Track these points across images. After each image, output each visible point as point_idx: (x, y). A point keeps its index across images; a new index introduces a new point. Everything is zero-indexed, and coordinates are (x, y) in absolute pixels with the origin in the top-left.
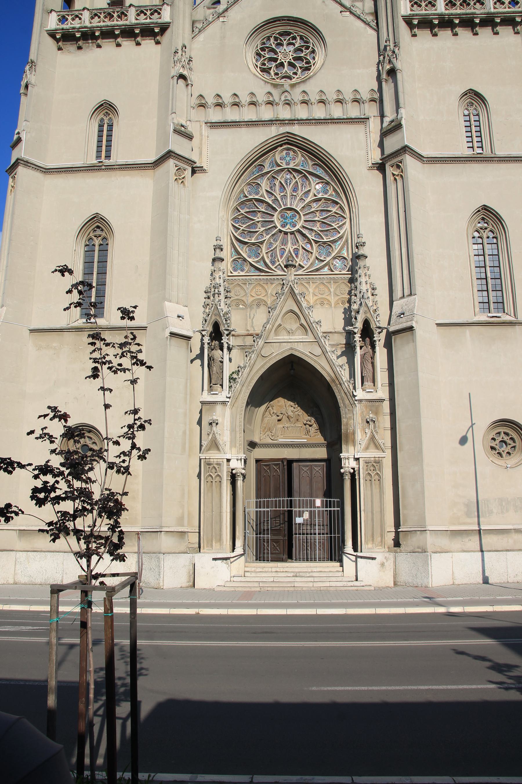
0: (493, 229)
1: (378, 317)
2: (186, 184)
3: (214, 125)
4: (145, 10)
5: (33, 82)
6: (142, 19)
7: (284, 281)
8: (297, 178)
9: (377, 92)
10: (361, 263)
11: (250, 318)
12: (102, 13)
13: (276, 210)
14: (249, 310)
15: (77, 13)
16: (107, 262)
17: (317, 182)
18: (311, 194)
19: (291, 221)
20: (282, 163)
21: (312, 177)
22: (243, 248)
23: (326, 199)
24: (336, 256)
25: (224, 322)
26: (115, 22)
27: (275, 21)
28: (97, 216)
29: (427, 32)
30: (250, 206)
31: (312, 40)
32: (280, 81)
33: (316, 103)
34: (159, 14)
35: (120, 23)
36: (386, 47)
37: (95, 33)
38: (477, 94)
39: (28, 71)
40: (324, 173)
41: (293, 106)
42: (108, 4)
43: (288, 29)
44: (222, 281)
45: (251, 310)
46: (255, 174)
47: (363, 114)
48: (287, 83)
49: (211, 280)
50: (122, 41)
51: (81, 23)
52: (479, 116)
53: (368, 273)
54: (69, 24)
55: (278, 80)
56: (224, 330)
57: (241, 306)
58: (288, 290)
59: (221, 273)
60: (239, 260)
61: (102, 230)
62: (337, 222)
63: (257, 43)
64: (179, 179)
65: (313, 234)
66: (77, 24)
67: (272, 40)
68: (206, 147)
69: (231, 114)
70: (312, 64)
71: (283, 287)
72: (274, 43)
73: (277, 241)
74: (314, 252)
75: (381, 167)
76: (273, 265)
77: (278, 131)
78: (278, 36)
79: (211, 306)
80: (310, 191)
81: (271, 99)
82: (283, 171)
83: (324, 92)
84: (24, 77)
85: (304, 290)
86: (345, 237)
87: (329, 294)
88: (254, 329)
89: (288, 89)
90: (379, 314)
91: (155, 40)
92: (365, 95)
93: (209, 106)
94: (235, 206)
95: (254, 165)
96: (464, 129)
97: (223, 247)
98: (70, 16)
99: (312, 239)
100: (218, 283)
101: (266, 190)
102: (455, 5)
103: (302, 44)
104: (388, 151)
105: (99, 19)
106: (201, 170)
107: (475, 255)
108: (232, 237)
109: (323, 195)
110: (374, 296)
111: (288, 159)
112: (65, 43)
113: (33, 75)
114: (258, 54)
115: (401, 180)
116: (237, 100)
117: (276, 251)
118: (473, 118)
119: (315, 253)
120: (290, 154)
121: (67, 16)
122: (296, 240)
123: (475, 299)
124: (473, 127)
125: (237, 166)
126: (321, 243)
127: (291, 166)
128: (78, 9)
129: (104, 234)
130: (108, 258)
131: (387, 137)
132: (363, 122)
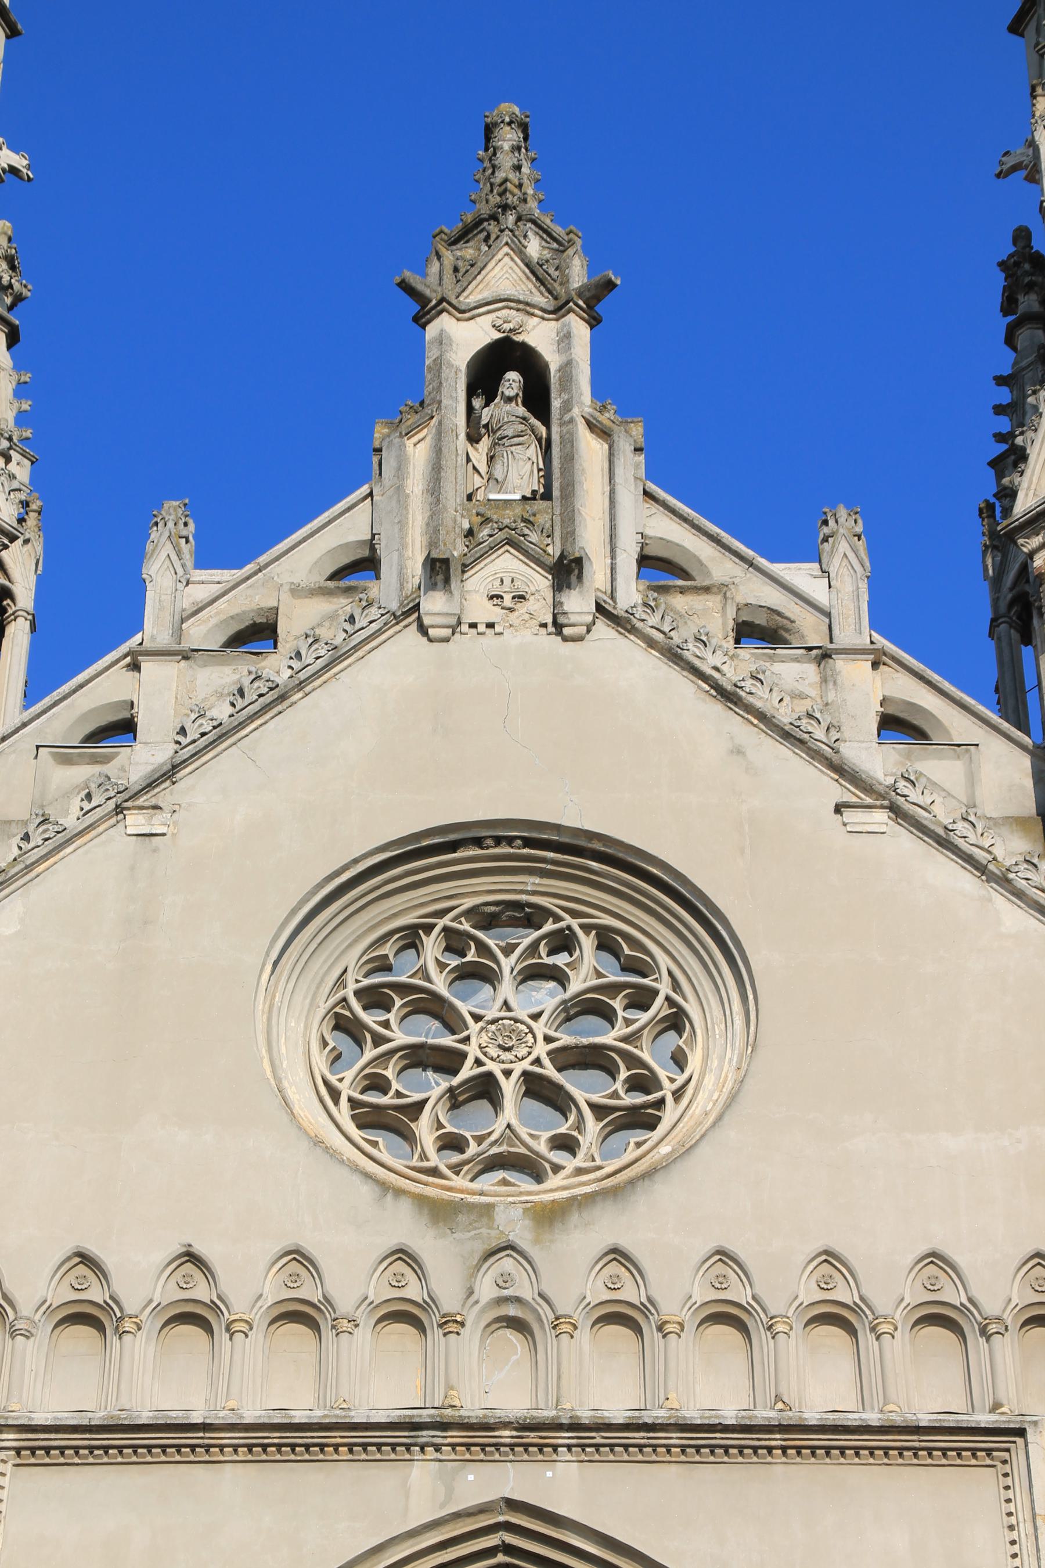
27: (453, 846)
32: (475, 1186)
33: (690, 1326)
41: (545, 1337)
47: (989, 1404)
55: (459, 1181)
67: (432, 946)
70: (667, 1089)
72: (441, 966)
78: (466, 926)
81: (414, 1291)
83: (742, 1255)
89: (521, 1233)
103: (612, 978)
116: (202, 1292)
132: (989, 1452)
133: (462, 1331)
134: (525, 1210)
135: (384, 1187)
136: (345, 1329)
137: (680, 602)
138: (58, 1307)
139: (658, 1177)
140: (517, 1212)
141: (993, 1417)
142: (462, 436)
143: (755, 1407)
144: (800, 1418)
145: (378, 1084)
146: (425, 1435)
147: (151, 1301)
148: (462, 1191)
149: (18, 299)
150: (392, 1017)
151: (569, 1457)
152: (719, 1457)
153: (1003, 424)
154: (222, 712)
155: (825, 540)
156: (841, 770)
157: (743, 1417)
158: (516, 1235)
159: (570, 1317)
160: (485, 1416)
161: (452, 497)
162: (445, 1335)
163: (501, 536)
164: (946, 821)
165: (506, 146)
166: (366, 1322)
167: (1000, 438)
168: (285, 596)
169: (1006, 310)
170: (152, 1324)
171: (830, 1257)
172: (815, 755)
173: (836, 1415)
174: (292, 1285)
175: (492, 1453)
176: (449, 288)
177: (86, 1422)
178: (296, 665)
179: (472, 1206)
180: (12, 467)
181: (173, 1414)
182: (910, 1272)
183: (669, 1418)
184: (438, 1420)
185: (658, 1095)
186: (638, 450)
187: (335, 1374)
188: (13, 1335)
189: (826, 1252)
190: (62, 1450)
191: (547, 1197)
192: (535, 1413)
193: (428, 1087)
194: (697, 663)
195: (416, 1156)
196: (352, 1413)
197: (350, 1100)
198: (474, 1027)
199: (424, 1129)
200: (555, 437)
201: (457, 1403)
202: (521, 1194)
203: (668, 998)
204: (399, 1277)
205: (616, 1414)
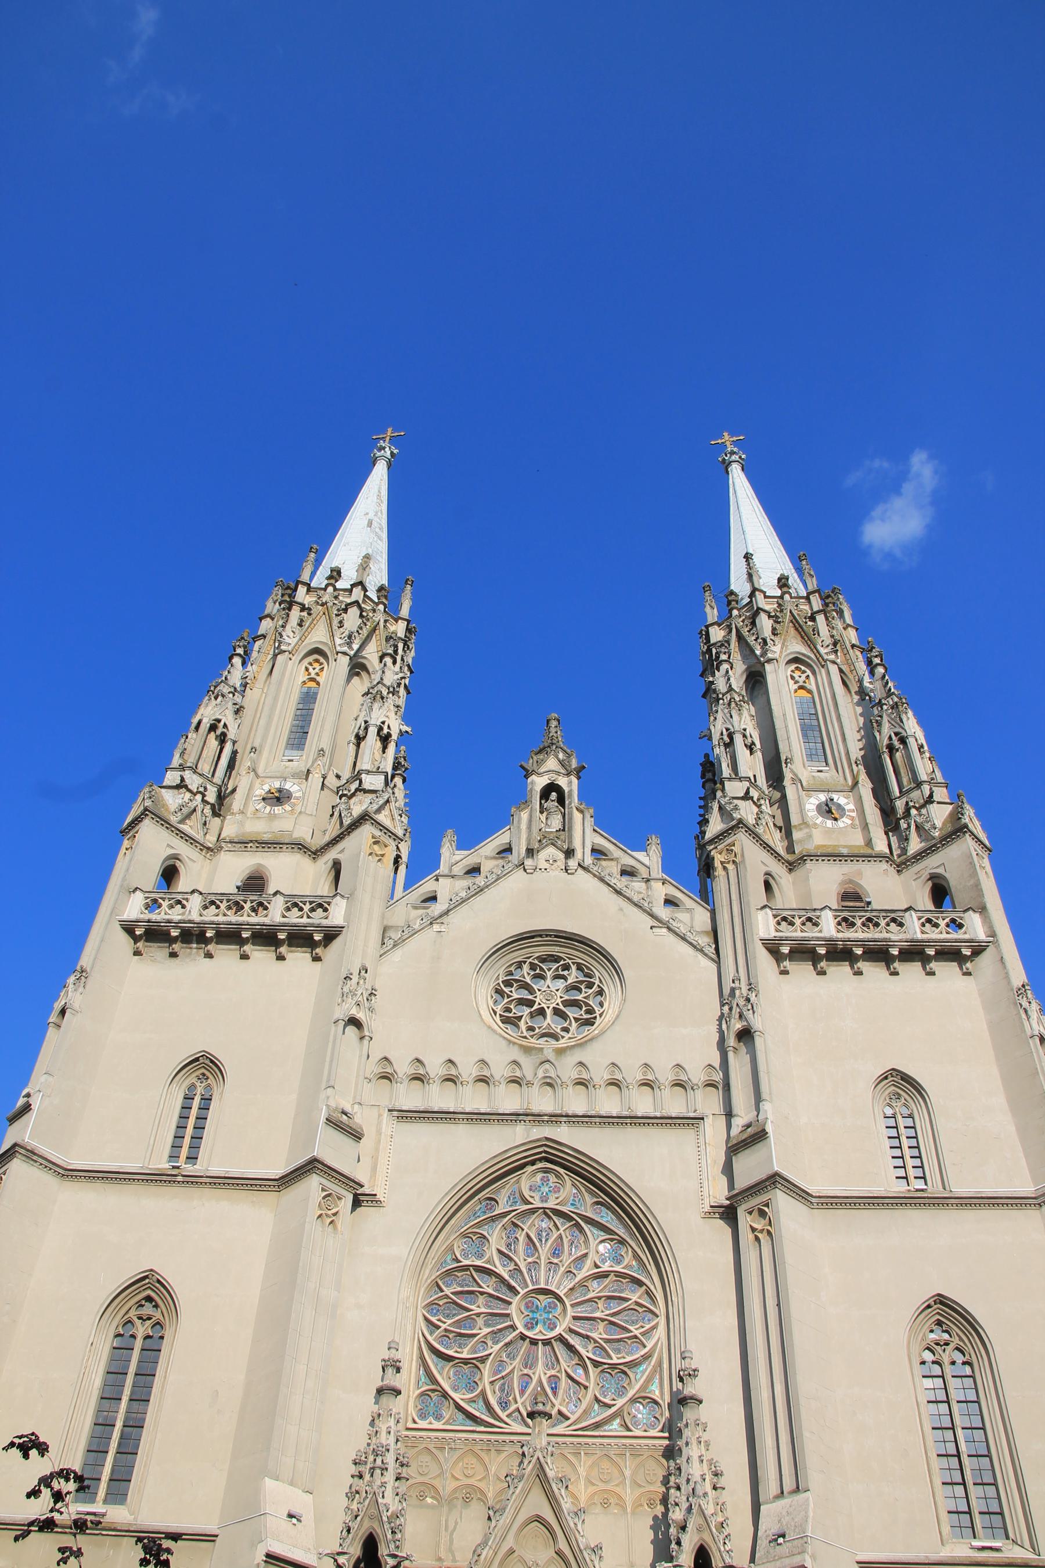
0: (961, 1344)
1: (727, 1542)
2: (339, 1226)
3: (405, 1116)
4: (301, 902)
5: (76, 1006)
6: (294, 918)
7: (525, 1449)
8: (562, 1229)
9: (718, 1069)
10: (689, 1414)
11: (446, 1530)
12: (225, 902)
13: (516, 1293)
14: (445, 1509)
15: (179, 897)
16: (154, 1375)
17: (601, 1238)
18: (589, 1263)
19: (545, 1316)
20: (531, 1197)
21: (592, 1229)
22: (443, 1368)
23: (619, 1274)
24: (636, 1396)
25: (389, 1536)
26: (245, 919)
27: (533, 937)
28: (150, 1276)
29: (808, 967)
30: (464, 1280)
31: (599, 973)
32: (537, 1042)
33: (603, 1086)
34: (326, 910)
35: (254, 919)
36: (733, 990)
37: (205, 932)
38: (906, 1078)
39: (71, 986)
40: (616, 1222)
41: (558, 1089)
42: (238, 888)
43: (555, 950)
44: (392, 1439)
45: (450, 1510)
46: (479, 1217)
47: (693, 1110)
48: (549, 1046)
49: (369, 1435)
50: (253, 950)
51: (183, 914)
52: (913, 1118)
53: (705, 1437)
54: (163, 913)
55: (532, 1040)
56: (388, 1555)
57: (429, 1500)
59: (392, 1422)
60: (432, 1395)
61: (156, 1306)
62: (641, 1324)
63: (499, 971)
64: (327, 1215)
65: (590, 1347)
66: (175, 914)
67: (526, 968)
68: (385, 1168)
69: (440, 1098)
70: (597, 1014)
71: (522, 1462)
72: (529, 974)
73: (514, 1358)
74: (592, 1385)
75: (729, 1214)
76: (504, 1409)
77: (528, 1136)
78: (536, 962)
79: (364, 1495)
80: (585, 1255)
81: (518, 1074)
82: (534, 1213)
83: (619, 1065)
84: (62, 994)
85: (568, 1471)
86: (656, 1355)
87: (621, 1482)
88: (453, 1556)
89: (551, 1057)
90: (729, 1535)
91: (312, 953)
92: (697, 1075)
93: (399, 1080)
94: (433, 1277)
95: (477, 1198)
96: (888, 1143)
97: (401, 1364)
98: (167, 900)
99: (588, 1358)
100: (385, 1444)
101: (498, 1250)
102: (853, 924)
103: (581, 979)
104: (742, 1182)
105: (218, 910)
106: (372, 1201)
107: (928, 1402)
108: (422, 1343)
109: (612, 1266)
110: (719, 1490)
111: (545, 1189)
112: (148, 944)
113: (78, 994)
114: (499, 992)
115: (767, 1241)
116: (453, 1072)
117: (512, 1379)
118: (902, 1123)
119: (593, 1389)
120: (549, 1180)
121: (160, 901)
122: (553, 1358)
123: (939, 1503)
124: (903, 1139)
125: (443, 1197)
126: (606, 1366)
127: (551, 1204)
128: (183, 891)
129: (157, 1315)
130: (159, 1368)
131: (739, 1155)
132: (693, 1124)
137: (604, 863)
139: (594, 1040)
141: (694, 1114)
142: (538, 812)
145: (508, 1010)
146: (521, 1118)
149: (406, 769)
150: (513, 989)
153: (702, 811)
154: (463, 894)
155: (648, 845)
156: (652, 916)
161: (535, 830)
163: (549, 842)
164: (684, 932)
165: (553, 726)
166: (504, 1083)
167: (701, 815)
168: (483, 859)
169: (702, 778)
172: (645, 911)
176: (535, 767)
178: (486, 880)
179: (537, 1048)
180: (403, 819)
185: (594, 1015)
186: (592, 817)
189: (645, 1064)
191: (560, 1046)
193: (524, 1011)
194: (609, 882)
197: (500, 1015)
198: (538, 993)
199: (522, 1024)
200: (566, 812)
203: (598, 985)
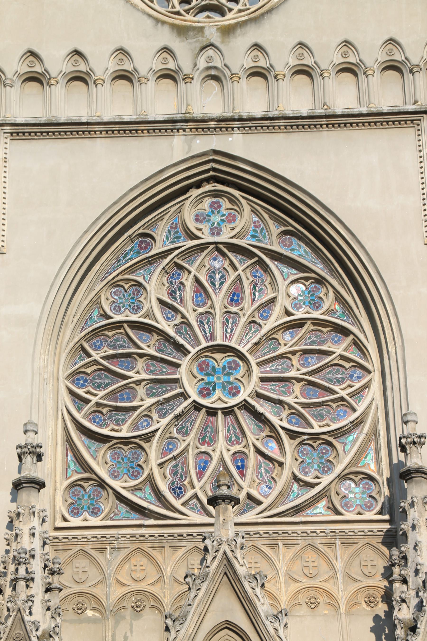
7: (208, 542)
32: (196, 19)
33: (288, 76)
41: (227, 83)
47: (412, 101)
55: (189, 17)
57: (90, 613)
58: (219, 566)
71: (204, 559)
81: (171, 65)
83: (310, 45)
89: (216, 38)
116: (82, 67)
132: (412, 121)
133: (192, 81)
134: (218, 29)
135: (157, 20)
136: (143, 82)
138: (23, 74)
139: (274, 12)
140: (214, 30)
143: (315, 108)
144: (334, 112)
146: (179, 125)
147: (61, 71)
148: (190, 21)
151: (238, 132)
152: (300, 129)
157: (310, 113)
158: (214, 40)
159: (238, 74)
160: (203, 117)
162: (185, 83)
166: (152, 79)
170: (63, 82)
171: (347, 43)
173: (349, 110)
174: (120, 64)
175: (206, 132)
177: (38, 122)
179: (195, 28)
181: (74, 118)
182: (381, 48)
183: (280, 114)
184: (184, 118)
187: (140, 101)
188: (5, 86)
189: (345, 41)
190: (30, 133)
192: (224, 115)
195: (170, 7)
196: (148, 117)
201: (191, 111)
202: (215, 22)
204: (165, 59)
205: (258, 114)
